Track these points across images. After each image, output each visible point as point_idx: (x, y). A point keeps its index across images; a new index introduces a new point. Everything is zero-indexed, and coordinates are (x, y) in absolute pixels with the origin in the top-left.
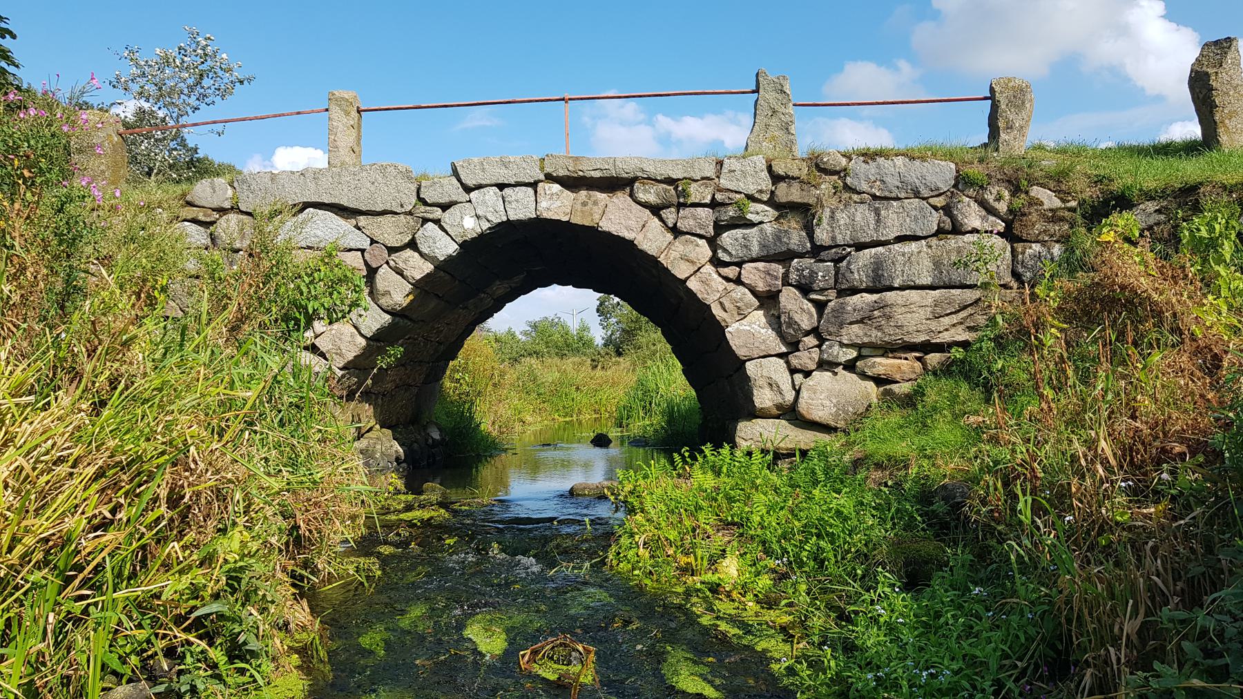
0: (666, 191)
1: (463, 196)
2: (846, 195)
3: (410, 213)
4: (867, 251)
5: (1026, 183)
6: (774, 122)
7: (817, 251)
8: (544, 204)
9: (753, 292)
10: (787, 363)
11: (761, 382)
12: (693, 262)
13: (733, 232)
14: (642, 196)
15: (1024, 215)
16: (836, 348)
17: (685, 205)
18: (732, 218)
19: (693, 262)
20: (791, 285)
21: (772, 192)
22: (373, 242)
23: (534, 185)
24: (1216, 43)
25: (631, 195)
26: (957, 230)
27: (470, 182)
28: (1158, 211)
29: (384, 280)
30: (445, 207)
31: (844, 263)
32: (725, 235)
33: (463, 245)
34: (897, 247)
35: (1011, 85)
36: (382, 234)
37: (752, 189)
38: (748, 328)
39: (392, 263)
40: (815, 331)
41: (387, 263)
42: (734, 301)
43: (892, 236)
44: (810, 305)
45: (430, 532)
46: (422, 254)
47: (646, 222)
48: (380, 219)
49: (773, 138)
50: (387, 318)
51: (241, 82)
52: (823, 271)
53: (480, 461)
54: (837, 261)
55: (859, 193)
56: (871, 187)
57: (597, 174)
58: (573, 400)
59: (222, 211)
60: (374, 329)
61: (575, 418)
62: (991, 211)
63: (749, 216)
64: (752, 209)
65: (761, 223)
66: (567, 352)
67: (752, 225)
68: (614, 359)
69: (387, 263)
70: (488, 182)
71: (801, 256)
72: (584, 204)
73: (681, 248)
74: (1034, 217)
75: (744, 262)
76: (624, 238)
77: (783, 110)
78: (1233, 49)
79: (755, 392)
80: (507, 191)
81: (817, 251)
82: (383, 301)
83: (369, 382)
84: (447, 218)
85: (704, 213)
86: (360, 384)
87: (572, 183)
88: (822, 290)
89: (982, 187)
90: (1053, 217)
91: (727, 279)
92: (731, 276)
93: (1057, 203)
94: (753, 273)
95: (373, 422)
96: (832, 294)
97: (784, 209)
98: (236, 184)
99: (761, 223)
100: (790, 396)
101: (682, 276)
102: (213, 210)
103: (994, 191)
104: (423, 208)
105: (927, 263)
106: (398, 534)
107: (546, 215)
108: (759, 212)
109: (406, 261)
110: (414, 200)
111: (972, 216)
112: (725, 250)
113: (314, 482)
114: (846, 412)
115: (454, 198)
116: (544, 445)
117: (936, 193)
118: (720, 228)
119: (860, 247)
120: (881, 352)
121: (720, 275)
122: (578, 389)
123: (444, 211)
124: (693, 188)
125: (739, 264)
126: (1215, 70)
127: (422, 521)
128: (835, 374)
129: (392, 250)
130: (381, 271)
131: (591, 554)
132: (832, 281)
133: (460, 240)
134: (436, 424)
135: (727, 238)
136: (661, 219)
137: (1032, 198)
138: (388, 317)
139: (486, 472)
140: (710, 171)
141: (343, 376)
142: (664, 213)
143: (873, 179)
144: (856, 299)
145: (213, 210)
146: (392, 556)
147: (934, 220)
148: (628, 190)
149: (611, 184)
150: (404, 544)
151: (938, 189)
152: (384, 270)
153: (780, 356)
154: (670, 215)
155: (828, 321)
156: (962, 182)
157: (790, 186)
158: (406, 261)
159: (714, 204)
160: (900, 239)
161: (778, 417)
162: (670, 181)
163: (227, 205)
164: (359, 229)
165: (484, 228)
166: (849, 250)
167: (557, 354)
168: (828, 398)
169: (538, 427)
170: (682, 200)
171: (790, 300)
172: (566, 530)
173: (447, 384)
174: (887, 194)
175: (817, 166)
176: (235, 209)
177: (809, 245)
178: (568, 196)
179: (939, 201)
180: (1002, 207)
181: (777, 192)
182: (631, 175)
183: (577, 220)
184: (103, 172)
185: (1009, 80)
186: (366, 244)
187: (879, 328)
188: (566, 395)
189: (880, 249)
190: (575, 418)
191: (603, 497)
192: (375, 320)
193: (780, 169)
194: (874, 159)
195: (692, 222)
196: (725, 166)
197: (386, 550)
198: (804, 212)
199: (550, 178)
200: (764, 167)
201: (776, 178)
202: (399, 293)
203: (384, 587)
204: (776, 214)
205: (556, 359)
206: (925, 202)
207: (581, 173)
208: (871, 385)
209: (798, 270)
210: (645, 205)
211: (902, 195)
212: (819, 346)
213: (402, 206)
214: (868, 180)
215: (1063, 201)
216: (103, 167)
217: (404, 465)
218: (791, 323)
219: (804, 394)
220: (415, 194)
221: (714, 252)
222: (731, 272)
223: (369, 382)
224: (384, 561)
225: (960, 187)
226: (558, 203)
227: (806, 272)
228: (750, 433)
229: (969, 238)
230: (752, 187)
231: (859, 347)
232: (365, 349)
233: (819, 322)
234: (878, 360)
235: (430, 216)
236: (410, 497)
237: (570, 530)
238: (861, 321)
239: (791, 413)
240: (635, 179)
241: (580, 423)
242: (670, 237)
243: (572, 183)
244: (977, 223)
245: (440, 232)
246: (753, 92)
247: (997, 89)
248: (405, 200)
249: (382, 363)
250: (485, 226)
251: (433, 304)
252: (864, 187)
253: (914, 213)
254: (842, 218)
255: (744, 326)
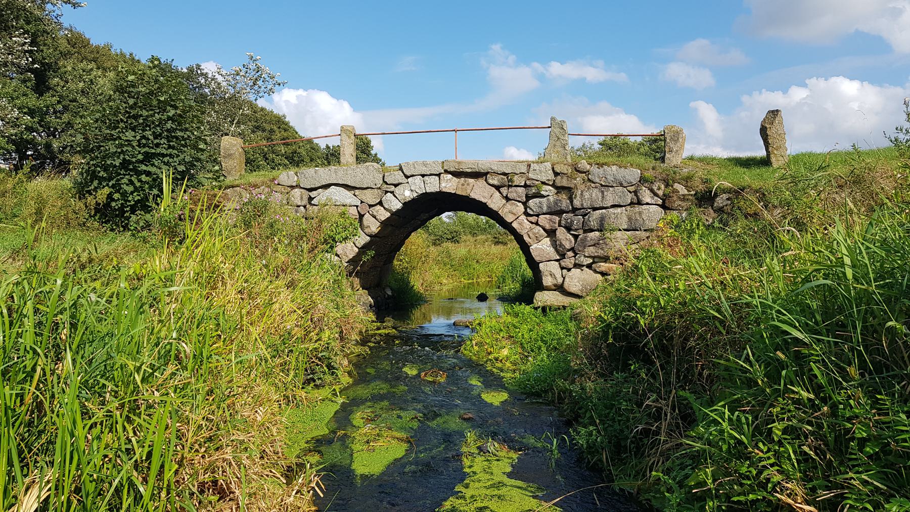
0: (502, 179)
1: (405, 180)
2: (589, 184)
3: (379, 188)
4: (597, 211)
5: (671, 182)
6: (558, 143)
7: (574, 210)
8: (443, 185)
9: (544, 229)
10: (560, 264)
11: (546, 273)
12: (515, 214)
13: (535, 199)
14: (491, 181)
15: (670, 197)
16: (583, 257)
17: (511, 186)
18: (534, 193)
19: (515, 214)
20: (562, 226)
21: (554, 181)
22: (362, 202)
23: (439, 175)
24: (773, 111)
25: (486, 180)
26: (639, 203)
27: (408, 174)
28: (728, 199)
29: (367, 220)
30: (396, 185)
31: (587, 217)
32: (530, 201)
33: (404, 204)
34: (611, 210)
35: (672, 129)
37: (544, 179)
38: (541, 247)
39: (370, 212)
40: (572, 249)
41: (368, 212)
42: (534, 234)
43: (609, 205)
44: (571, 236)
45: (389, 338)
46: (384, 208)
47: (493, 194)
49: (557, 152)
51: (279, 84)
52: (577, 220)
53: (413, 307)
54: (584, 216)
55: (594, 183)
56: (600, 181)
57: (469, 170)
58: (474, 269)
59: (292, 187)
60: (362, 244)
61: (475, 281)
62: (656, 195)
63: (542, 193)
64: (544, 189)
65: (548, 196)
66: (477, 232)
67: (543, 196)
68: (510, 237)
69: (368, 212)
70: (417, 174)
71: (567, 212)
72: (463, 185)
73: (509, 207)
74: (675, 198)
75: (540, 215)
76: (482, 202)
77: (562, 138)
78: (779, 115)
79: (543, 278)
80: (426, 178)
81: (574, 210)
82: (366, 231)
83: (359, 268)
84: (397, 191)
85: (520, 190)
86: (354, 269)
88: (576, 230)
89: (652, 182)
90: (683, 198)
91: (532, 223)
92: (533, 221)
93: (686, 192)
94: (544, 220)
95: (359, 286)
96: (581, 232)
97: (559, 189)
98: (298, 174)
99: (548, 196)
100: (560, 280)
101: (509, 221)
102: (288, 187)
103: (657, 185)
104: (386, 186)
105: (625, 219)
106: (375, 339)
107: (444, 190)
108: (548, 190)
109: (377, 211)
110: (381, 182)
111: (647, 197)
112: (531, 209)
113: (346, 315)
114: (586, 289)
115: (400, 181)
116: (449, 299)
117: (630, 184)
118: (528, 198)
119: (595, 209)
120: (604, 260)
121: (528, 220)
122: (477, 262)
123: (395, 187)
124: (516, 178)
125: (538, 216)
126: (770, 126)
127: (385, 334)
128: (582, 270)
129: (371, 206)
130: (366, 216)
131: (454, 348)
132: (581, 225)
133: (403, 202)
134: (389, 286)
135: (531, 203)
136: (500, 192)
137: (674, 189)
138: (368, 238)
139: (417, 313)
140: (524, 170)
141: (347, 266)
142: (502, 190)
143: (601, 176)
144: (592, 235)
145: (288, 187)
146: (373, 347)
147: (629, 198)
148: (484, 178)
149: (476, 175)
150: (379, 343)
151: (631, 183)
152: (367, 216)
153: (557, 260)
154: (504, 191)
155: (579, 245)
156: (643, 180)
157: (562, 178)
158: (377, 211)
159: (526, 186)
160: (613, 206)
161: (555, 290)
162: (504, 174)
163: (294, 184)
164: (355, 196)
165: (415, 196)
166: (589, 210)
167: (470, 233)
168: (578, 282)
169: (451, 287)
170: (510, 184)
171: (561, 233)
172: (446, 339)
173: (395, 262)
174: (607, 184)
175: (575, 169)
176: (298, 186)
177: (571, 207)
178: (455, 181)
179: (632, 189)
180: (660, 193)
181: (556, 181)
182: (486, 171)
183: (459, 193)
184: (235, 166)
185: (672, 127)
186: (359, 203)
187: (602, 249)
188: (470, 266)
189: (604, 211)
190: (475, 281)
191: (467, 326)
192: (363, 239)
193: (558, 170)
194: (602, 167)
195: (515, 195)
196: (532, 167)
197: (372, 345)
198: (568, 191)
199: (446, 172)
200: (550, 168)
201: (556, 174)
202: (374, 227)
203: (371, 356)
204: (556, 191)
205: (469, 236)
206: (625, 189)
207: (461, 170)
208: (599, 276)
209: (565, 219)
210: (492, 185)
211: (615, 185)
212: (575, 257)
213: (376, 185)
214: (599, 177)
215: (688, 191)
216: (235, 164)
217: (374, 308)
218: (561, 245)
219: (567, 279)
220: (382, 179)
221: (526, 209)
222: (533, 219)
223: (359, 268)
224: (371, 348)
225: (642, 182)
226: (450, 184)
227: (569, 221)
228: (542, 298)
229: (645, 207)
230: (544, 178)
231: (593, 257)
232: (358, 253)
233: (575, 244)
234: (602, 264)
235: (389, 190)
236: (379, 324)
237: (449, 339)
238: (594, 245)
239: (560, 288)
240: (488, 173)
241: (478, 284)
242: (504, 201)
243: (457, 174)
244: (648, 200)
245: (394, 198)
246: (549, 127)
247: (666, 131)
248: (377, 182)
249: (364, 259)
250: (415, 195)
251: (390, 229)
252: (597, 180)
253: (619, 194)
254: (587, 195)
255: (539, 246)
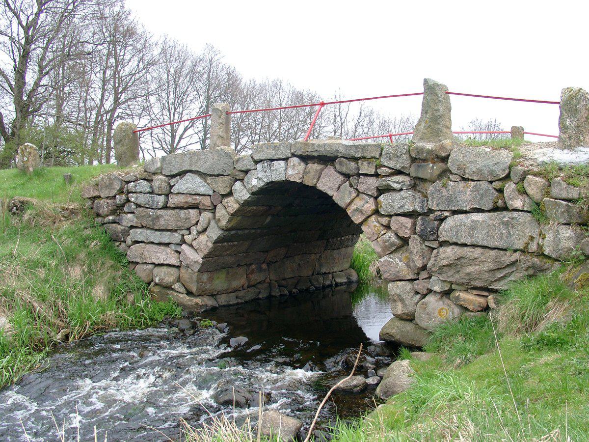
23: (286, 159)
36: (217, 187)
48: (217, 179)
50: (221, 232)
57: (316, 154)
87: (306, 159)
115: (249, 167)
222: (384, 221)
